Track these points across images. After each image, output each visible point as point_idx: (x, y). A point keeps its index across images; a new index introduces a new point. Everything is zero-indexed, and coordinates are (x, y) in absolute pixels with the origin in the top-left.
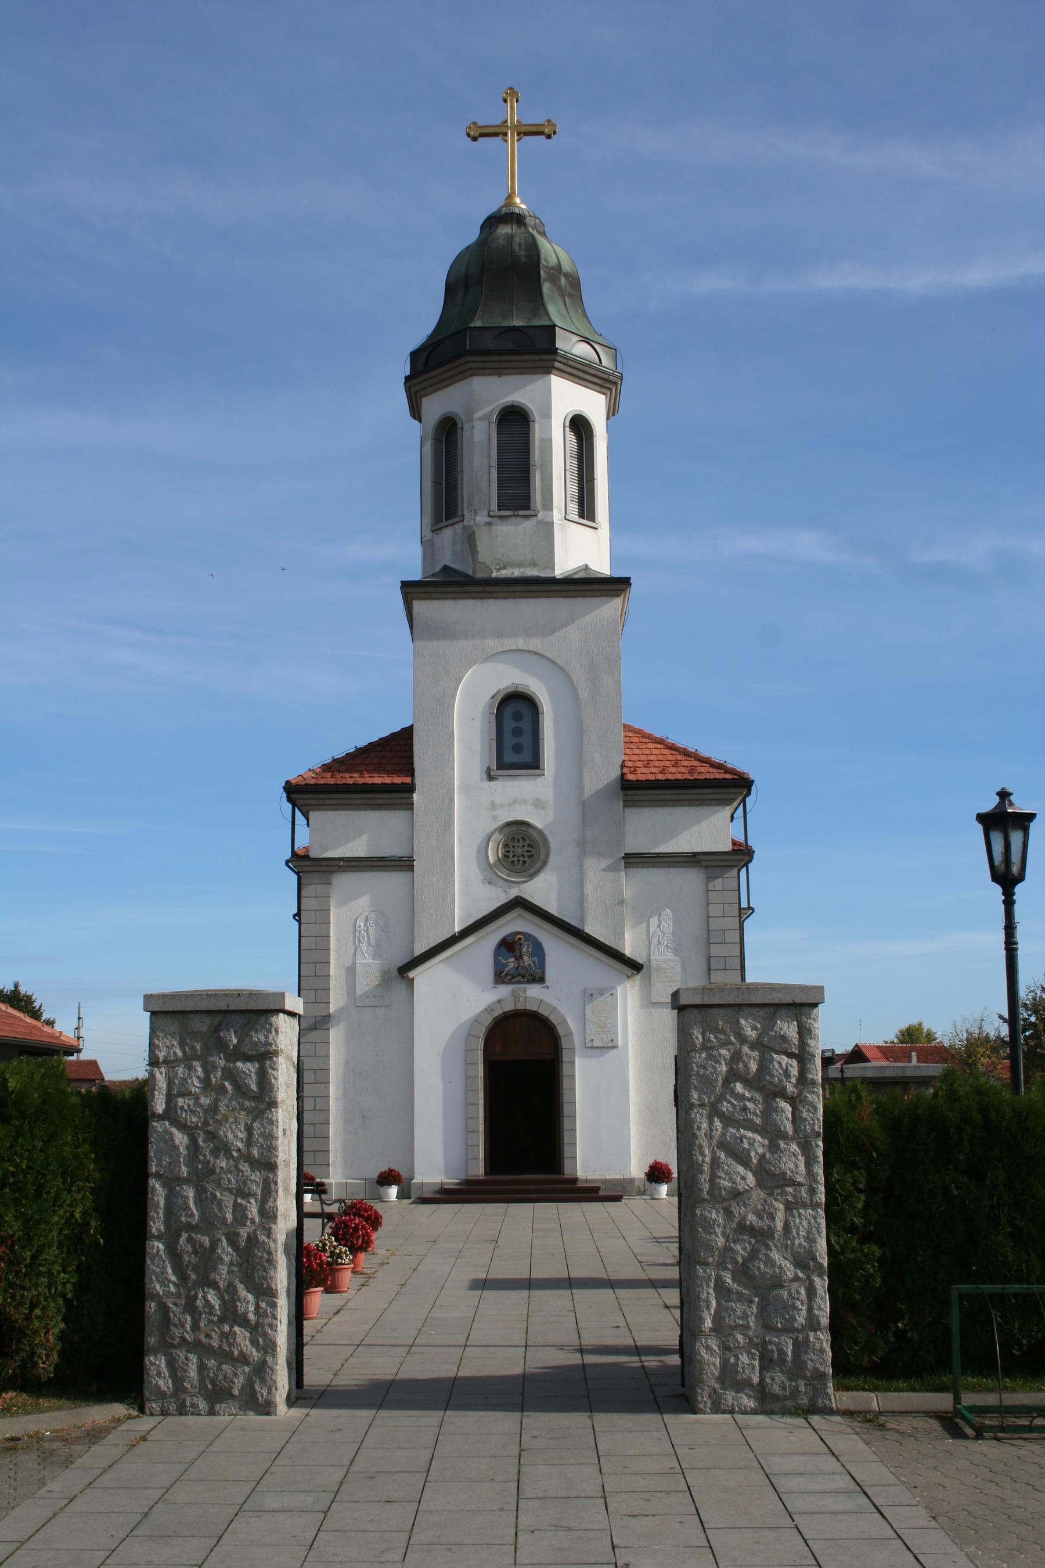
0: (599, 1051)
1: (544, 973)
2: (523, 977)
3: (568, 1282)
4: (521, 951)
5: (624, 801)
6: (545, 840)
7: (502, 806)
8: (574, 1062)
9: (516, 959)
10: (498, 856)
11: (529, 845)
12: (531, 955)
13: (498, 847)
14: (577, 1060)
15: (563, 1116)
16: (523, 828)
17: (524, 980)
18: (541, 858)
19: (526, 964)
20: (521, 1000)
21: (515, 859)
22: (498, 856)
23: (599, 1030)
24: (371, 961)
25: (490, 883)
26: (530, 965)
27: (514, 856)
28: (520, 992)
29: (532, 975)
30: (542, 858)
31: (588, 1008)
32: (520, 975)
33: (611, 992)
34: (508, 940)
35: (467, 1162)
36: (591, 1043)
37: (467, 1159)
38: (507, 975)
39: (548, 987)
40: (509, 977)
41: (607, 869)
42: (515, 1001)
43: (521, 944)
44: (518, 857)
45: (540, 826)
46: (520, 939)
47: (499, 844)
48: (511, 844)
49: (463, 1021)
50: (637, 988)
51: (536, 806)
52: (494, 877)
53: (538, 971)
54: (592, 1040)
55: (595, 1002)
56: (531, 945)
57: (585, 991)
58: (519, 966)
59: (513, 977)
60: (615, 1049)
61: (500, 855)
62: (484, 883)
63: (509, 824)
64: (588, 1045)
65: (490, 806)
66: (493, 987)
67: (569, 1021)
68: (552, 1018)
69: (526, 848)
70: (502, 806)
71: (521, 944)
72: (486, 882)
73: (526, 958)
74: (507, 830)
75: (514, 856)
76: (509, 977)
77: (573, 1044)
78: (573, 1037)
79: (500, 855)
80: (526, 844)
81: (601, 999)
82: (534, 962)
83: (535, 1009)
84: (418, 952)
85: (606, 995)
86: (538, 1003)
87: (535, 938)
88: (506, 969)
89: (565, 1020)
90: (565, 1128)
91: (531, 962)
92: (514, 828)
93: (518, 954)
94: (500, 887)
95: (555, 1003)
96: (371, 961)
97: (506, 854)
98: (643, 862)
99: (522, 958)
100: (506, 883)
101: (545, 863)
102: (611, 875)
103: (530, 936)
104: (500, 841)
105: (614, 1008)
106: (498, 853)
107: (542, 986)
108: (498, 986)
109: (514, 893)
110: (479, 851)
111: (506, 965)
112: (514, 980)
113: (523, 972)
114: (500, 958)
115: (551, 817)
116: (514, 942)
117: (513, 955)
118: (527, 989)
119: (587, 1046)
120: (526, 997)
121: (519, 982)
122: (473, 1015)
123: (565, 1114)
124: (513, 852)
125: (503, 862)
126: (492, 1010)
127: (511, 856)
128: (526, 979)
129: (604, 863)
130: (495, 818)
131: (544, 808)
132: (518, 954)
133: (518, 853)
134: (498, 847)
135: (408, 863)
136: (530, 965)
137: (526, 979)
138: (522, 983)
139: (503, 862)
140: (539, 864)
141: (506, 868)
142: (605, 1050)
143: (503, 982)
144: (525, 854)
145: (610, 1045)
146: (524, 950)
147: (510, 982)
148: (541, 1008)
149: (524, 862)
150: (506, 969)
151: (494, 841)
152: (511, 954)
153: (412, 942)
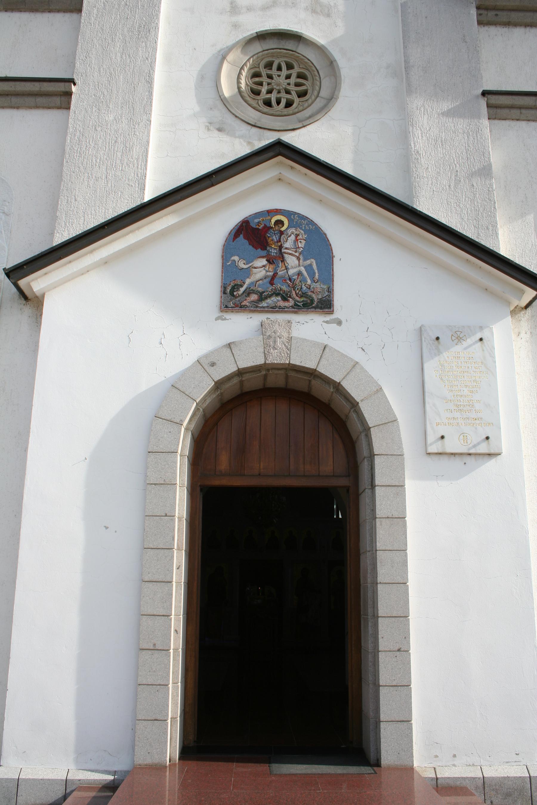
0: (457, 462)
1: (330, 291)
2: (285, 299)
3: (161, 578)
4: (281, 247)
5: (478, 8)
6: (331, 63)
7: (249, 9)
8: (403, 486)
9: (270, 261)
10: (239, 88)
11: (300, 76)
12: (305, 254)
13: (240, 73)
14: (410, 485)
15: (376, 617)
16: (290, 45)
17: (286, 304)
18: (321, 94)
19: (291, 272)
20: (279, 344)
21: (273, 97)
22: (239, 88)
23: (457, 415)
25: (220, 130)
26: (299, 274)
27: (270, 92)
28: (276, 327)
29: (304, 295)
30: (324, 93)
31: (430, 367)
32: (277, 295)
33: (479, 336)
34: (253, 225)
35: (134, 730)
36: (440, 442)
37: (136, 720)
38: (248, 293)
39: (339, 323)
40: (254, 297)
41: (448, 114)
42: (266, 346)
43: (282, 233)
44: (279, 92)
45: (321, 41)
46: (280, 223)
47: (242, 68)
48: (264, 72)
49: (144, 387)
50: (525, 336)
51: (314, 11)
52: (230, 120)
53: (318, 286)
54: (443, 437)
55: (445, 354)
56: (303, 236)
57: (421, 330)
58: (275, 274)
59: (262, 297)
60: (499, 456)
61: (243, 85)
62: (209, 129)
63: (262, 36)
64: (431, 449)
65: (228, 9)
66: (217, 319)
67: (387, 391)
68: (349, 386)
69: (274, 72)
70: (249, 9)
71: (282, 233)
72: (211, 128)
73: (291, 261)
74: (257, 47)
75: (270, 92)
76: (254, 297)
77: (400, 447)
78: (398, 427)
79: (243, 85)
80: (294, 73)
81: (458, 348)
82: (309, 268)
83: (310, 364)
84: (59, 239)
85: (469, 341)
86: (319, 352)
87: (311, 222)
88: (248, 281)
89: (380, 390)
90: (383, 645)
91: (302, 269)
92: (271, 44)
93: (274, 252)
94: (240, 137)
95: (357, 356)
97: (255, 87)
98: (520, 108)
99: (283, 261)
100: (254, 130)
101: (331, 99)
102: (462, 124)
103: (303, 217)
104: (245, 64)
105: (491, 371)
106: (239, 82)
107: (328, 318)
108: (227, 316)
109: (269, 138)
110: (201, 77)
111: (248, 272)
112: (264, 304)
113: (284, 288)
114: (236, 258)
115: (340, 31)
116: (267, 228)
117: (264, 253)
118: (294, 324)
119: (430, 450)
120: (290, 339)
121: (274, 309)
122: (168, 376)
123: (382, 610)
124: (269, 84)
125: (248, 99)
126: (213, 364)
127: (289, 96)
128: (291, 303)
129: (446, 106)
130: (236, 26)
131: (328, 15)
132: (274, 252)
133: (278, 85)
134: (240, 73)
135: (61, 87)
136: (299, 274)
137: (291, 303)
138: (281, 310)
139: (248, 99)
140: (318, 103)
141: (254, 108)
142: (468, 459)
143: (240, 307)
144: (292, 88)
145: (483, 448)
146: (287, 245)
147: (255, 308)
148: (323, 362)
149: (289, 104)
150: (248, 281)
151: (233, 64)
152: (260, 252)
153: (54, 218)
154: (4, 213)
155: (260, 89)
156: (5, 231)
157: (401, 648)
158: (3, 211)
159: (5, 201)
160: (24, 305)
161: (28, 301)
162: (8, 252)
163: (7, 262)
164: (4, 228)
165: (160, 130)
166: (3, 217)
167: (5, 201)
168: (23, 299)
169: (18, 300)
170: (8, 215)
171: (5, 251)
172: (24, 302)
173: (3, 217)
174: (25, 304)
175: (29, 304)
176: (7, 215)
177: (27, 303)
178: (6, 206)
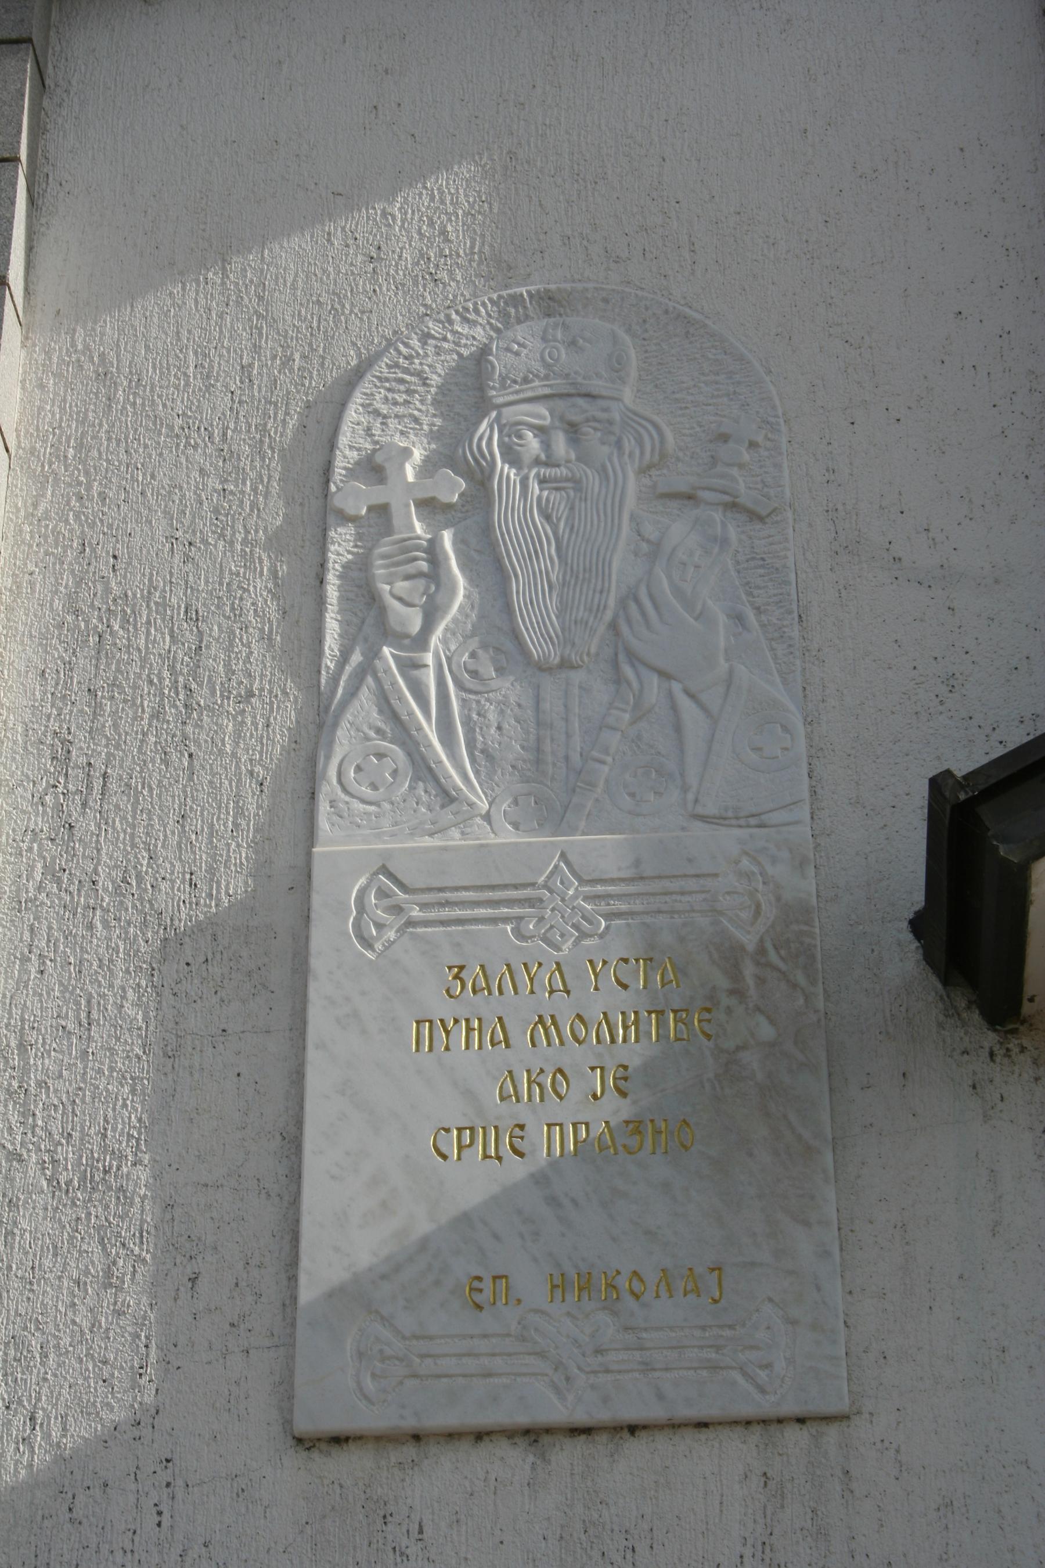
24: (508, 836)
96: (508, 836)
154: (733, 506)
155: (948, 808)
156: (758, 610)
157: (563, 718)
158: (727, 498)
159: (724, 438)
160: (992, 1055)
161: (1014, 1032)
162: (809, 737)
163: (814, 793)
164: (750, 594)
165: (663, 1293)
166: (733, 533)
167: (724, 438)
168: (976, 1016)
169: (941, 1026)
170: (761, 519)
171: (785, 729)
172: (990, 1039)
173: (733, 533)
174: (1000, 1052)
175: (1023, 1049)
176: (754, 516)
177: (1013, 1044)
178: (741, 466)
